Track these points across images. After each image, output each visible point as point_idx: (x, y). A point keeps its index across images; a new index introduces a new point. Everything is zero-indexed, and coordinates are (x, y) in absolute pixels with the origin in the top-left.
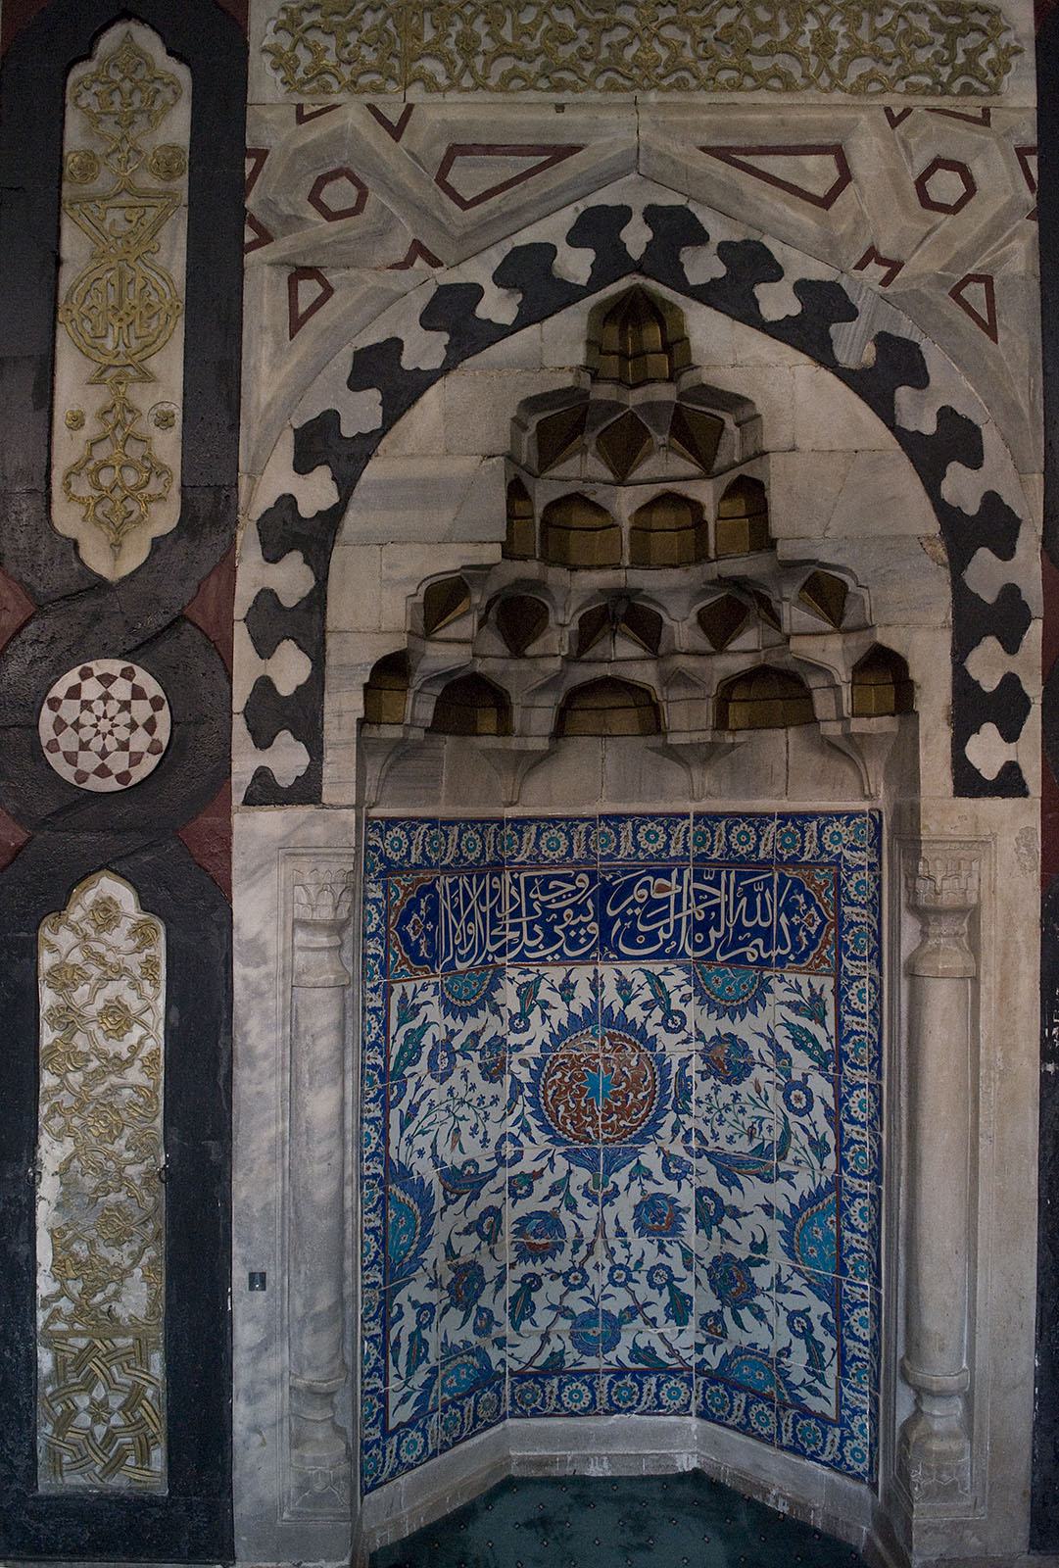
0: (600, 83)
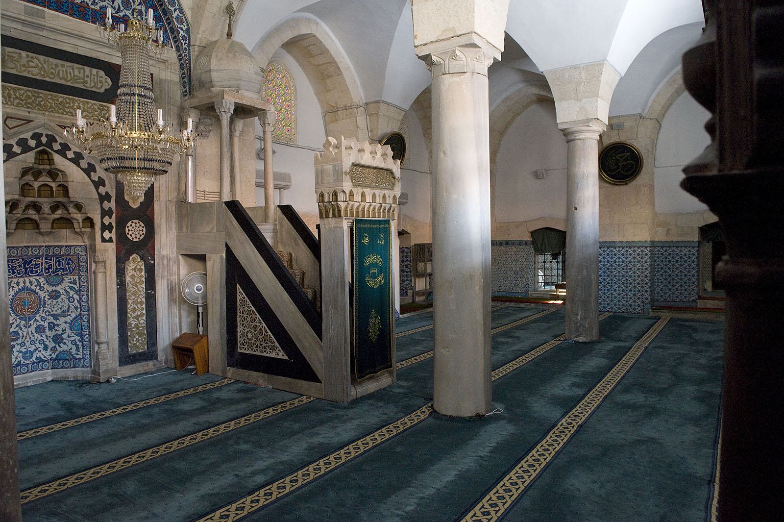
0: (37, 108)
